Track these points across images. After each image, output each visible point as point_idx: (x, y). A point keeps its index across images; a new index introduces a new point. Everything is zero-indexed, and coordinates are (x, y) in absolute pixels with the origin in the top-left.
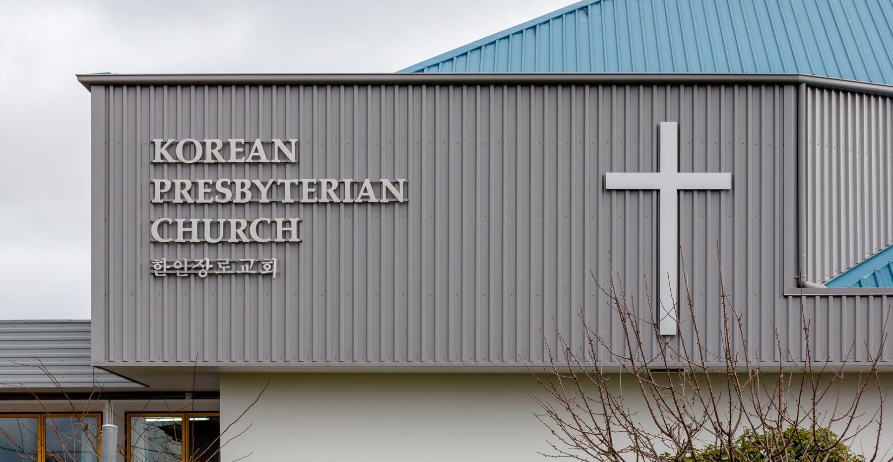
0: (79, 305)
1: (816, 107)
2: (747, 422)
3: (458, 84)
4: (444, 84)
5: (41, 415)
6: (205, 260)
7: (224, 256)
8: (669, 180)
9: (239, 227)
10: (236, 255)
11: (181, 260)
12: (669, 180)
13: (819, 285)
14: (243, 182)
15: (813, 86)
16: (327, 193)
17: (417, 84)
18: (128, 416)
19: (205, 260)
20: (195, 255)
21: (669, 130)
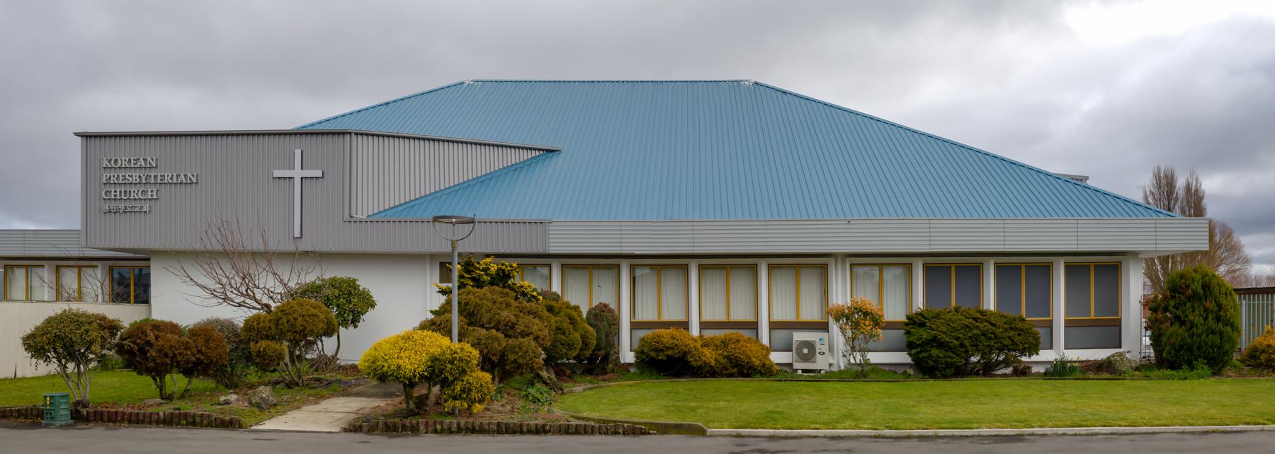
0: (77, 225)
1: (361, 144)
2: (310, 275)
3: (317, 134)
4: (312, 134)
5: (27, 267)
6: (122, 206)
7: (128, 204)
8: (297, 173)
9: (135, 192)
10: (133, 204)
11: (113, 205)
12: (297, 173)
13: (359, 216)
14: (136, 174)
15: (356, 134)
16: (167, 180)
17: (301, 134)
18: (58, 268)
19: (122, 206)
20: (118, 203)
21: (298, 153)
